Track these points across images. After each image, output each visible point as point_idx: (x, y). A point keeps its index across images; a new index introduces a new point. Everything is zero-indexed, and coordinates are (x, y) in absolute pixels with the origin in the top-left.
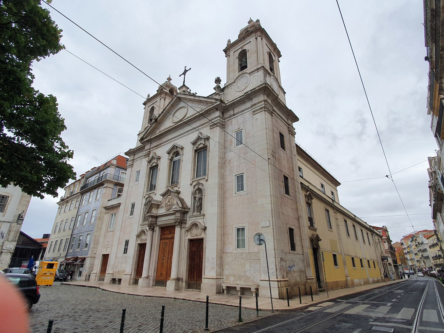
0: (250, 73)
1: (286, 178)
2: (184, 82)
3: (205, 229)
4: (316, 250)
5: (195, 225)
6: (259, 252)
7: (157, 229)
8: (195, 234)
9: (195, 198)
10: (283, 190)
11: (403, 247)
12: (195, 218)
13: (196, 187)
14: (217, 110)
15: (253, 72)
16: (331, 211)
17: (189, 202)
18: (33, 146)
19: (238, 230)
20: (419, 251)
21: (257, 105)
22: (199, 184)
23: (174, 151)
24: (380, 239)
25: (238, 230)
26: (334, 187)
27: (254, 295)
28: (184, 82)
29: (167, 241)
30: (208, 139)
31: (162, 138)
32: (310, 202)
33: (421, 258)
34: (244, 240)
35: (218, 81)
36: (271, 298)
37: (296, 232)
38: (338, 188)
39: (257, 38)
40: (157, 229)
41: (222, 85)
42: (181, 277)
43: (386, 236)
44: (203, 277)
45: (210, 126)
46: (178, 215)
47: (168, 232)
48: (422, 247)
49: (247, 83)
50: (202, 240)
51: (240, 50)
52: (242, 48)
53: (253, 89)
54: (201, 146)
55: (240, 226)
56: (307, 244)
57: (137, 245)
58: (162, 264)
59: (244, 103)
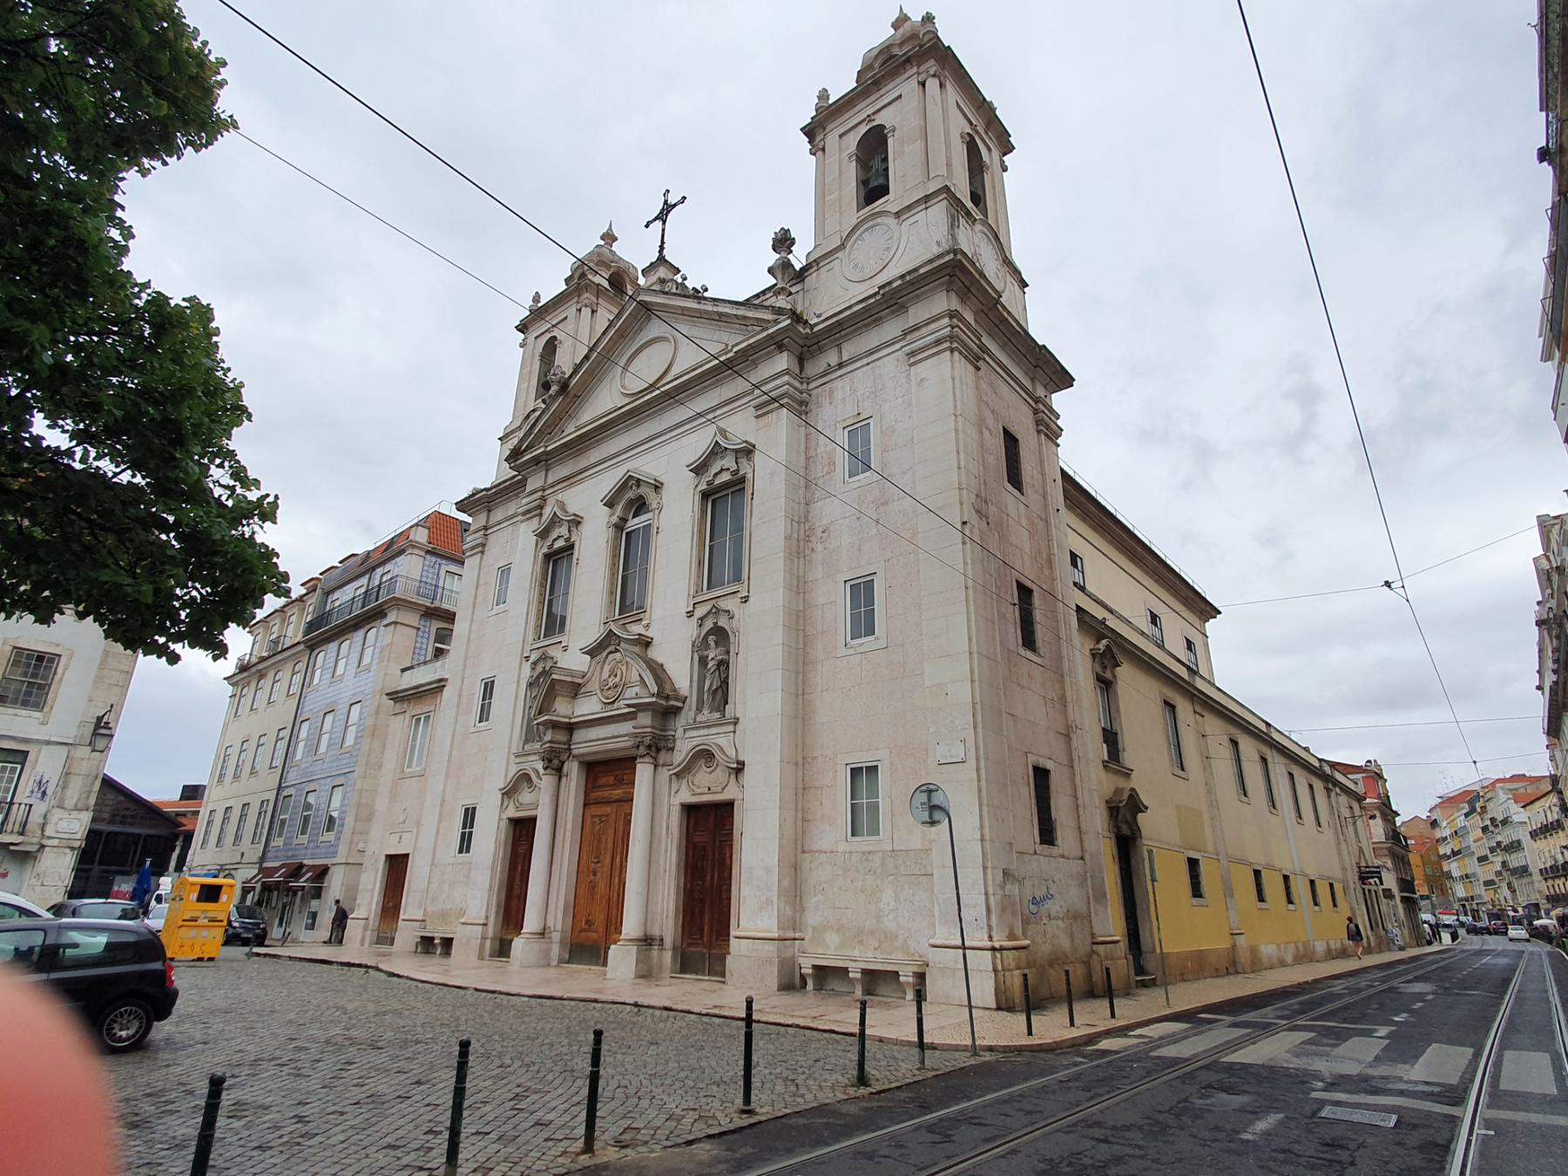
0: (898, 215)
1: (1025, 592)
2: (662, 248)
3: (739, 769)
4: (1126, 843)
5: (705, 755)
6: (928, 851)
7: (573, 769)
8: (706, 786)
9: (703, 661)
10: (1014, 634)
11: (1438, 834)
12: (705, 732)
13: (708, 625)
14: (781, 347)
15: (909, 208)
16: (1184, 708)
17: (682, 675)
18: (138, 479)
19: (855, 772)
20: (1492, 850)
21: (924, 331)
22: (716, 611)
23: (630, 495)
24: (1356, 806)
25: (855, 772)
26: (1196, 622)
27: (910, 995)
28: (662, 248)
29: (607, 809)
30: (748, 451)
31: (588, 448)
32: (1108, 675)
33: (1499, 874)
34: (874, 808)
35: (783, 242)
36: (970, 1007)
37: (1058, 782)
38: (1210, 626)
39: (923, 84)
40: (573, 769)
41: (798, 259)
42: (656, 932)
43: (1379, 797)
44: (733, 933)
45: (757, 407)
46: (645, 719)
47: (611, 780)
48: (1504, 836)
49: (888, 249)
50: (729, 806)
51: (864, 129)
52: (869, 119)
53: (909, 273)
54: (726, 477)
55: (862, 759)
56: (1097, 821)
57: (504, 823)
58: (593, 887)
59: (878, 321)
